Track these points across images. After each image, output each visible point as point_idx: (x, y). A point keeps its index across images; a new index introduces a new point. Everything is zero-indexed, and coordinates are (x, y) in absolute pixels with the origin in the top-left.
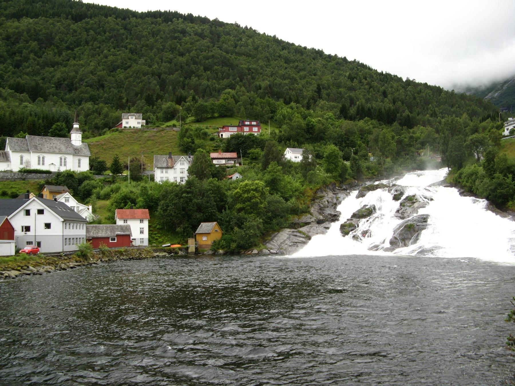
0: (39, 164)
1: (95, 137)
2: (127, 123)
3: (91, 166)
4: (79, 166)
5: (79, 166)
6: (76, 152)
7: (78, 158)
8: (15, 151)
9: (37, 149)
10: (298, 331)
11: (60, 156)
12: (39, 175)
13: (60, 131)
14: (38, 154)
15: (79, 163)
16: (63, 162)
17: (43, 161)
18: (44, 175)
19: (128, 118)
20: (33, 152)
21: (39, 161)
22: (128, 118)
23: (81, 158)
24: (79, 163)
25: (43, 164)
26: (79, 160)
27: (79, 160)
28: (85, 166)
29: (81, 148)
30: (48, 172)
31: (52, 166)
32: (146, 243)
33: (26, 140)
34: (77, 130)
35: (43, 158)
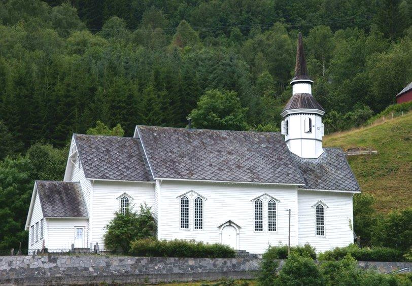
7: (314, 201)
14: (180, 191)
17: (199, 213)
21: (184, 212)
26: (320, 211)
27: (320, 211)
31: (229, 230)
35: (199, 203)
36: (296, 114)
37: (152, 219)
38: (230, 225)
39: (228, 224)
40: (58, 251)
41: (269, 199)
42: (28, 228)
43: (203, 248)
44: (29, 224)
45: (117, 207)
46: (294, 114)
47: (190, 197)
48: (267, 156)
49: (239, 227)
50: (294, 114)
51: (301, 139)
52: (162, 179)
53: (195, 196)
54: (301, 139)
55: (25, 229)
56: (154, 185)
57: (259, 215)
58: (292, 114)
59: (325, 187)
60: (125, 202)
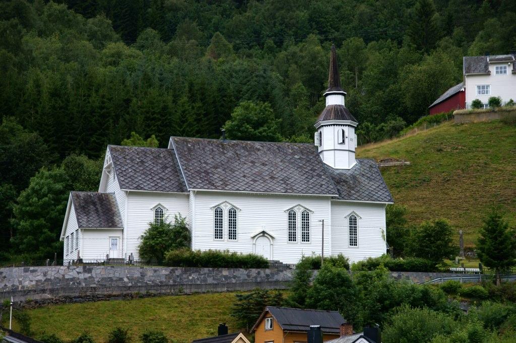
0: (218, 234)
1: (182, 136)
2: (483, 89)
3: (394, 240)
4: (353, 242)
5: (353, 242)
6: (342, 189)
7: (347, 211)
8: (135, 190)
9: (209, 184)
10: (169, 309)
11: (288, 205)
12: (225, 272)
13: (257, 125)
14: (215, 202)
15: (353, 230)
16: (298, 228)
17: (233, 224)
18: (242, 273)
19: (488, 74)
20: (198, 194)
21: (218, 223)
22: (488, 74)
23: (361, 213)
24: (353, 230)
25: (233, 235)
26: (353, 221)
27: (353, 221)
28: (371, 242)
29: (354, 177)
30: (256, 263)
31: (263, 241)
32: (55, 238)
33: (171, 154)
34: (338, 114)
35: (233, 214)
36: (329, 125)
37: (186, 229)
38: (263, 236)
39: (262, 235)
40: (92, 262)
41: (302, 209)
42: (63, 238)
43: (237, 258)
44: (64, 235)
45: (151, 217)
46: (327, 125)
47: (224, 208)
48: (301, 167)
49: (272, 238)
50: (327, 125)
51: (335, 150)
52: (196, 190)
53: (229, 207)
54: (335, 150)
55: (61, 239)
56: (188, 196)
57: (292, 226)
58: (325, 126)
59: (359, 198)
60: (159, 212)
